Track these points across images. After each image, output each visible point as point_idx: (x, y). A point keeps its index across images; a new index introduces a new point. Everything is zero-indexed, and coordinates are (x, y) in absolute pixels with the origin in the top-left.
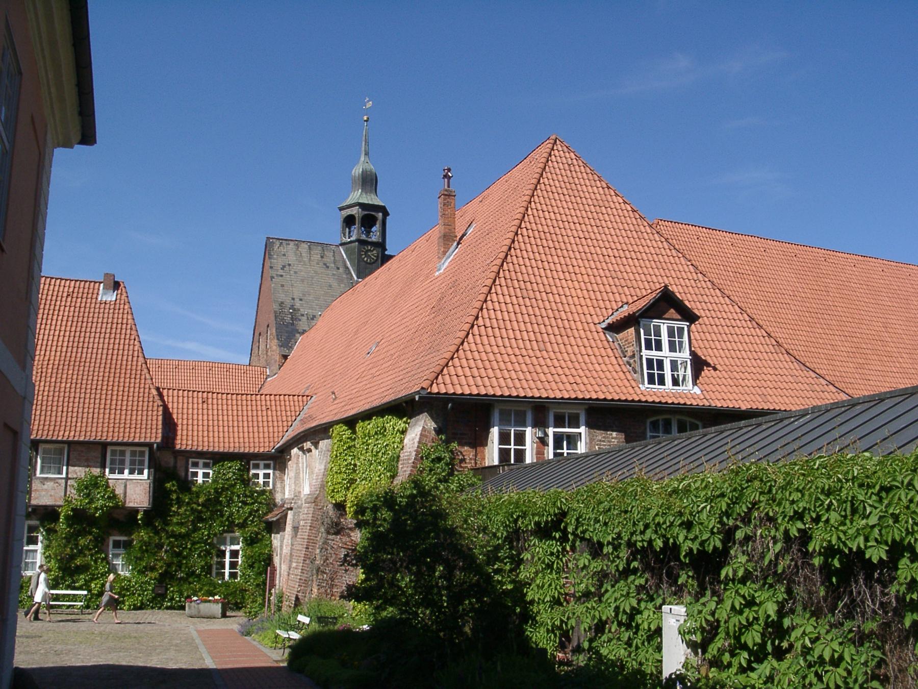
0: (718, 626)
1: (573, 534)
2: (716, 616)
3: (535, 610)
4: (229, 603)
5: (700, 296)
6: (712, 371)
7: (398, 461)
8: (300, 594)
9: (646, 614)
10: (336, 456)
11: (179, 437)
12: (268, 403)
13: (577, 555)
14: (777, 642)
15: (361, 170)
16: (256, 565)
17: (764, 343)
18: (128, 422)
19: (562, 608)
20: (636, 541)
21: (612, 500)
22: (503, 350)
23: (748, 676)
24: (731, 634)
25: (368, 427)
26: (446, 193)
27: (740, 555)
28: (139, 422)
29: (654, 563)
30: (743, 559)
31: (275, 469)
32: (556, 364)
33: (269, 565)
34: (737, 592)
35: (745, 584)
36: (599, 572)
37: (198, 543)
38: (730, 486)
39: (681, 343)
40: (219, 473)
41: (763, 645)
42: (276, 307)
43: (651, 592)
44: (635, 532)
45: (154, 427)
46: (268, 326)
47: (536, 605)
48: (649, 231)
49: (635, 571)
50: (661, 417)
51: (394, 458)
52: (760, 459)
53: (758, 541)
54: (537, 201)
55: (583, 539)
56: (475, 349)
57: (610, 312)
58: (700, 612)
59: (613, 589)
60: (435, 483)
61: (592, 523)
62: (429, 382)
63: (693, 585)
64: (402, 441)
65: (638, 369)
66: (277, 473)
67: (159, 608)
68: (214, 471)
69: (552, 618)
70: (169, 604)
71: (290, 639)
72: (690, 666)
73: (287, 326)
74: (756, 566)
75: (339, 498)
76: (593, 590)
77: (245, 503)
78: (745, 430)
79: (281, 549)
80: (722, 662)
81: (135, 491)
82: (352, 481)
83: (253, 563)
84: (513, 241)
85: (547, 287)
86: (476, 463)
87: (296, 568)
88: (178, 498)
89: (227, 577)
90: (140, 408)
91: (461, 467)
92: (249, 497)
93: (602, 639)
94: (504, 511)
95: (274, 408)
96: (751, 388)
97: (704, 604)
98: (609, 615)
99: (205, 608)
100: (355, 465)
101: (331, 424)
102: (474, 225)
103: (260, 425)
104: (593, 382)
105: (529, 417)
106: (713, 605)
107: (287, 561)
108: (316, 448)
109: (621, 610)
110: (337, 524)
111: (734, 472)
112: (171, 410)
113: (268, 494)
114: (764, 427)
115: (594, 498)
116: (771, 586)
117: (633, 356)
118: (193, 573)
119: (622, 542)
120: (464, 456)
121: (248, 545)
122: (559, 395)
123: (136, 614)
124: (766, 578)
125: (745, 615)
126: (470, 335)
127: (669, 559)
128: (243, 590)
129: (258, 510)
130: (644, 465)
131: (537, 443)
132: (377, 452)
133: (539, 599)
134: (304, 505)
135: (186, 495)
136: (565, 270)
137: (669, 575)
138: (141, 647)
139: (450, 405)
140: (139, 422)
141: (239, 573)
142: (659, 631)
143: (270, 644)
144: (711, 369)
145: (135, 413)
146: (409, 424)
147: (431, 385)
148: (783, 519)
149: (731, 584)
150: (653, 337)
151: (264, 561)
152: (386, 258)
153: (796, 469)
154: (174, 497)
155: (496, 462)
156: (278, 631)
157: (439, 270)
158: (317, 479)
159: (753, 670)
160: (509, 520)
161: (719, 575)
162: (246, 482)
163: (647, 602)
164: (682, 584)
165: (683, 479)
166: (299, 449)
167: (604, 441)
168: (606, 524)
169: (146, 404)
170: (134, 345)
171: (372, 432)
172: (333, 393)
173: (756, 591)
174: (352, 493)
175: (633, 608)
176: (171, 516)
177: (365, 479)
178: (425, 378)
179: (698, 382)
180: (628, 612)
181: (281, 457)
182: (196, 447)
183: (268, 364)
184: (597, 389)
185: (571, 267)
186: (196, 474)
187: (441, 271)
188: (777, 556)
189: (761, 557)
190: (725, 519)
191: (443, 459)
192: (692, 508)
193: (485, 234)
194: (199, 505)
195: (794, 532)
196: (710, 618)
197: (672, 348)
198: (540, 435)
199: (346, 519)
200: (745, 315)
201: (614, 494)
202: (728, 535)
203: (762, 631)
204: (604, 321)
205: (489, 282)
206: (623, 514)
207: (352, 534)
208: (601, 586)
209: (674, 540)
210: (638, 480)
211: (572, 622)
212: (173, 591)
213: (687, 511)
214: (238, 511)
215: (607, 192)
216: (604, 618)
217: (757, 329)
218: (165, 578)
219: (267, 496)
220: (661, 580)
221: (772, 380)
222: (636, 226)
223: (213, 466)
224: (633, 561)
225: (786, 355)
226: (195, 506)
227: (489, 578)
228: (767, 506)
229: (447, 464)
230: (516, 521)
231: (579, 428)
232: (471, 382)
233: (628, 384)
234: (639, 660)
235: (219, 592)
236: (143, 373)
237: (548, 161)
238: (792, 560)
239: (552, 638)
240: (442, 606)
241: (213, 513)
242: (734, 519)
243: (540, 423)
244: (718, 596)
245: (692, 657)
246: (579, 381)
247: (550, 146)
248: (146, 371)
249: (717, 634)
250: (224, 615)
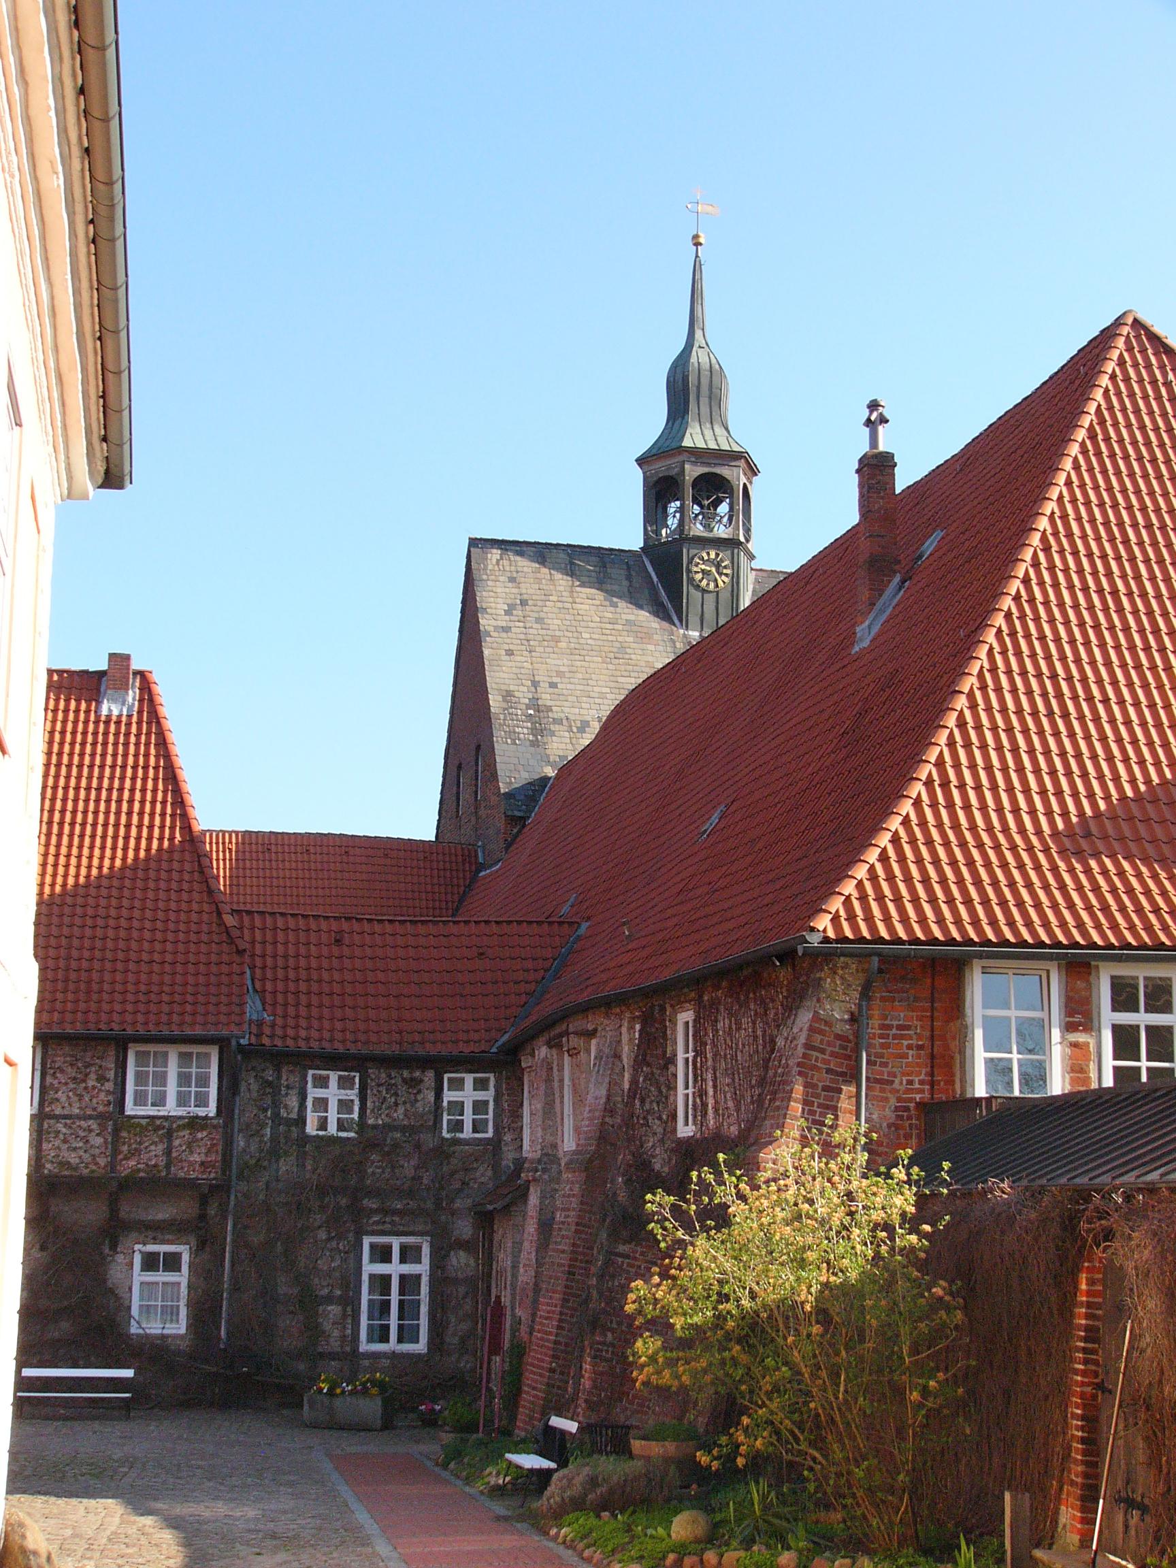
158: (590, 1119)
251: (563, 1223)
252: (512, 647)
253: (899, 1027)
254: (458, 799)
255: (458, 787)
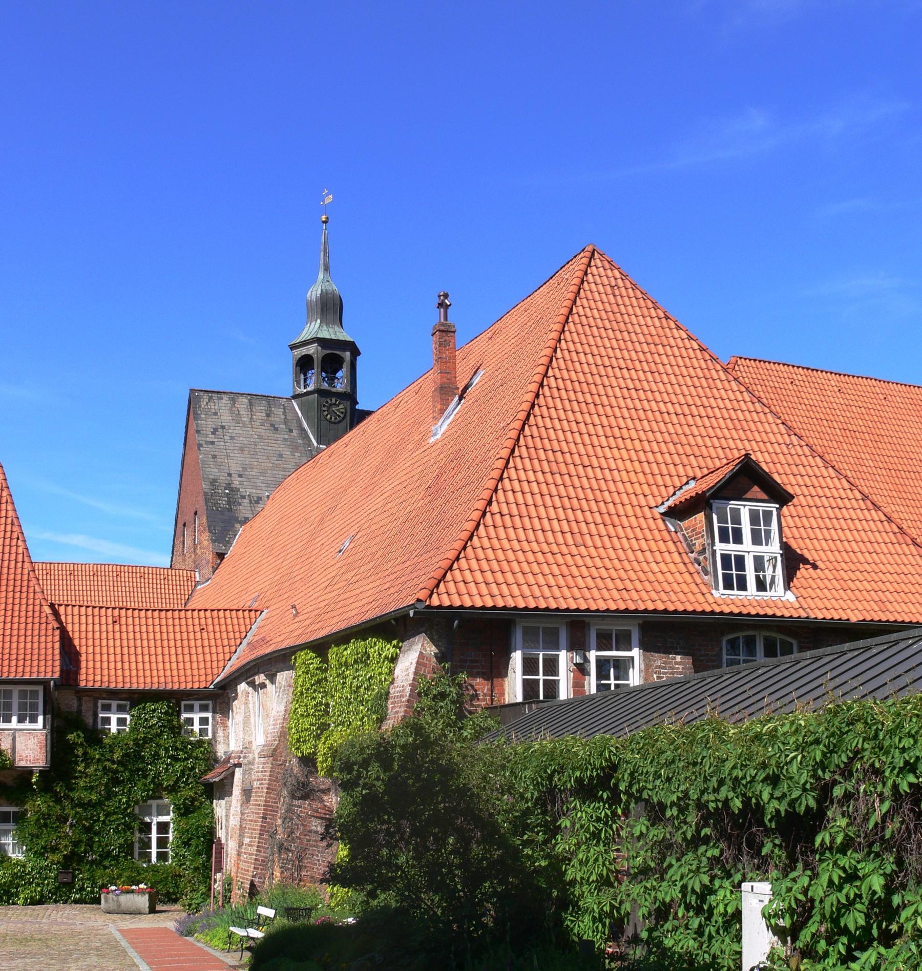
0: (812, 907)
1: (626, 793)
2: (810, 894)
3: (577, 893)
4: (157, 892)
5: (793, 467)
6: (811, 570)
7: (386, 700)
8: (257, 880)
9: (721, 893)
10: (302, 694)
11: (83, 671)
12: (203, 621)
13: (631, 821)
14: (884, 924)
15: (319, 292)
16: (193, 842)
17: (882, 530)
18: (14, 651)
19: (612, 890)
20: (708, 801)
21: (676, 749)
22: (526, 546)
23: (848, 968)
24: (827, 916)
25: (345, 653)
26: (442, 328)
27: (839, 817)
28: (29, 651)
29: (731, 829)
30: (842, 822)
31: (214, 712)
32: (599, 563)
33: (211, 842)
34: (835, 863)
35: (845, 854)
36: (660, 842)
37: (114, 813)
38: (827, 729)
39: (768, 533)
40: (139, 718)
41: (867, 929)
42: (205, 486)
43: (728, 867)
44: (706, 789)
45: (50, 657)
46: (196, 513)
47: (578, 886)
48: (723, 377)
49: (706, 840)
50: (741, 634)
51: (382, 695)
52: (866, 695)
53: (861, 799)
54: (569, 338)
55: (638, 800)
56: (489, 546)
57: (671, 490)
58: (789, 890)
59: (679, 863)
60: (442, 729)
61: (651, 778)
62: (427, 592)
63: (780, 857)
64: (391, 672)
65: (710, 568)
66: (218, 717)
67: (65, 902)
68: (133, 716)
69: (600, 903)
70: (78, 896)
71: (249, 938)
72: (776, 957)
73: (222, 513)
74: (859, 831)
75: (307, 749)
76: (653, 865)
77: (175, 759)
78: (850, 655)
79: (227, 821)
80: (817, 952)
81: (26, 745)
82: (324, 727)
83: (190, 839)
84: (537, 396)
85: (585, 457)
86: (492, 700)
87: (250, 845)
88: (85, 753)
89: (154, 859)
90: (29, 633)
91: (472, 705)
92: (181, 750)
93: (665, 927)
94: (535, 764)
95: (210, 628)
96: (864, 592)
97: (794, 880)
98: (674, 896)
99: (126, 900)
100: (327, 705)
101: (293, 650)
102: (481, 372)
103: (193, 651)
104: (649, 588)
105: (563, 637)
106: (805, 881)
107: (236, 836)
108: (273, 682)
109: (689, 889)
110: (305, 785)
111: (831, 712)
112: (71, 634)
113: (206, 745)
114: (874, 651)
115: (653, 746)
116: (877, 855)
117: (703, 551)
118: (109, 853)
119: (691, 802)
120: (476, 691)
121: (181, 815)
122: (603, 606)
123: (34, 910)
124: (870, 845)
125: (844, 891)
126: (482, 527)
127: (750, 823)
128: (176, 876)
129: (193, 768)
130: (718, 703)
131: (574, 671)
132: (358, 688)
133: (582, 878)
134: (257, 760)
135: (96, 750)
136: (609, 434)
137: (750, 844)
138: (52, 952)
139: (456, 622)
140: (29, 651)
141: (170, 853)
142: (737, 915)
143: (221, 945)
144: (809, 566)
145: (22, 639)
146: (400, 648)
147: (430, 596)
148: (892, 771)
149: (828, 854)
150: (730, 525)
151: (204, 836)
152: (359, 416)
153: (908, 708)
154: (80, 751)
155: (519, 699)
156: (232, 929)
157: (435, 434)
159: (855, 959)
160: (541, 777)
161: (813, 842)
162: (176, 730)
163: (722, 878)
164: (767, 855)
165: (769, 721)
166: (248, 683)
167: (664, 668)
168: (669, 780)
169: (36, 626)
170: (17, 546)
171: (351, 661)
172: (294, 607)
173: (858, 862)
174: (324, 743)
175: (704, 886)
176: (76, 778)
177: (342, 723)
178: (421, 586)
179: (792, 585)
180: (699, 891)
181: (223, 694)
182: (106, 684)
183: (197, 566)
184: (654, 596)
185: (616, 429)
186: (107, 721)
187: (438, 436)
188: (884, 817)
189: (864, 819)
190: (820, 772)
191: (449, 695)
192: (779, 758)
193: (497, 385)
194: (113, 762)
195: (904, 787)
196: (801, 897)
197: (756, 540)
198: (579, 660)
199: (316, 778)
200: (856, 492)
201: (679, 741)
202: (824, 792)
203: (866, 911)
204: (663, 503)
205: (505, 453)
206: (691, 767)
207: (326, 798)
208: (663, 860)
209: (757, 799)
210: (710, 723)
211: (627, 907)
212: (82, 879)
213: (773, 762)
214: (167, 770)
215: (665, 325)
216: (668, 900)
217: (873, 512)
218: (71, 861)
219: (205, 749)
220: (740, 850)
221: (892, 580)
222: (706, 371)
223: (130, 709)
224: (704, 827)
225: (912, 546)
226: (108, 764)
227: (515, 853)
228: (873, 756)
229: (453, 702)
230: (550, 778)
231: (630, 650)
232: (484, 590)
233: (696, 590)
234: (712, 952)
235: (144, 879)
236: (31, 584)
237: (582, 282)
238: (902, 823)
239: (600, 929)
240: (455, 890)
241: (133, 773)
242: (831, 772)
243: (578, 645)
244: (812, 870)
245: (779, 946)
246: (630, 586)
247: (585, 260)
248: (34, 581)
249: (810, 917)
250: (152, 910)
251: (259, 788)
252: (215, 453)
253: (472, 661)
254: (184, 544)
255: (184, 537)
